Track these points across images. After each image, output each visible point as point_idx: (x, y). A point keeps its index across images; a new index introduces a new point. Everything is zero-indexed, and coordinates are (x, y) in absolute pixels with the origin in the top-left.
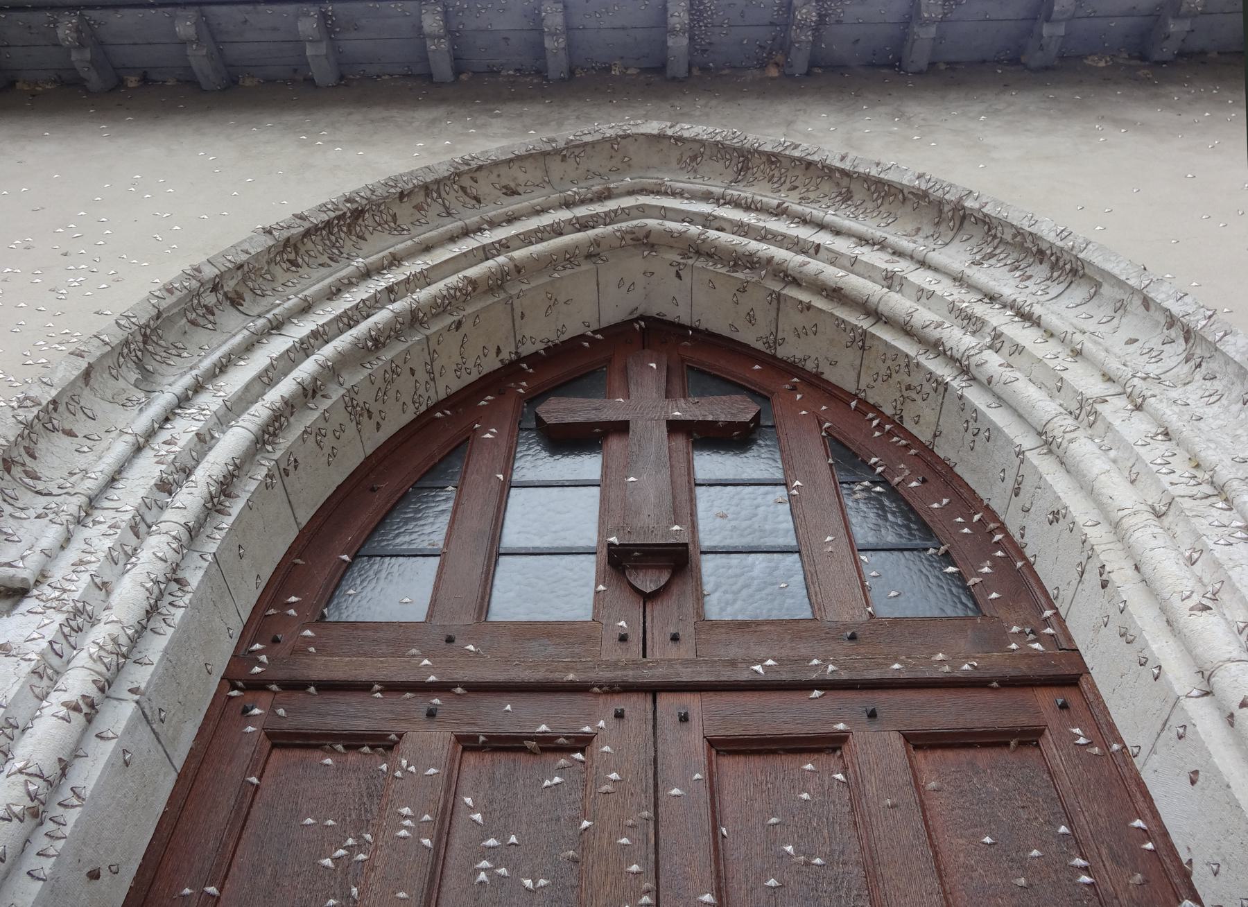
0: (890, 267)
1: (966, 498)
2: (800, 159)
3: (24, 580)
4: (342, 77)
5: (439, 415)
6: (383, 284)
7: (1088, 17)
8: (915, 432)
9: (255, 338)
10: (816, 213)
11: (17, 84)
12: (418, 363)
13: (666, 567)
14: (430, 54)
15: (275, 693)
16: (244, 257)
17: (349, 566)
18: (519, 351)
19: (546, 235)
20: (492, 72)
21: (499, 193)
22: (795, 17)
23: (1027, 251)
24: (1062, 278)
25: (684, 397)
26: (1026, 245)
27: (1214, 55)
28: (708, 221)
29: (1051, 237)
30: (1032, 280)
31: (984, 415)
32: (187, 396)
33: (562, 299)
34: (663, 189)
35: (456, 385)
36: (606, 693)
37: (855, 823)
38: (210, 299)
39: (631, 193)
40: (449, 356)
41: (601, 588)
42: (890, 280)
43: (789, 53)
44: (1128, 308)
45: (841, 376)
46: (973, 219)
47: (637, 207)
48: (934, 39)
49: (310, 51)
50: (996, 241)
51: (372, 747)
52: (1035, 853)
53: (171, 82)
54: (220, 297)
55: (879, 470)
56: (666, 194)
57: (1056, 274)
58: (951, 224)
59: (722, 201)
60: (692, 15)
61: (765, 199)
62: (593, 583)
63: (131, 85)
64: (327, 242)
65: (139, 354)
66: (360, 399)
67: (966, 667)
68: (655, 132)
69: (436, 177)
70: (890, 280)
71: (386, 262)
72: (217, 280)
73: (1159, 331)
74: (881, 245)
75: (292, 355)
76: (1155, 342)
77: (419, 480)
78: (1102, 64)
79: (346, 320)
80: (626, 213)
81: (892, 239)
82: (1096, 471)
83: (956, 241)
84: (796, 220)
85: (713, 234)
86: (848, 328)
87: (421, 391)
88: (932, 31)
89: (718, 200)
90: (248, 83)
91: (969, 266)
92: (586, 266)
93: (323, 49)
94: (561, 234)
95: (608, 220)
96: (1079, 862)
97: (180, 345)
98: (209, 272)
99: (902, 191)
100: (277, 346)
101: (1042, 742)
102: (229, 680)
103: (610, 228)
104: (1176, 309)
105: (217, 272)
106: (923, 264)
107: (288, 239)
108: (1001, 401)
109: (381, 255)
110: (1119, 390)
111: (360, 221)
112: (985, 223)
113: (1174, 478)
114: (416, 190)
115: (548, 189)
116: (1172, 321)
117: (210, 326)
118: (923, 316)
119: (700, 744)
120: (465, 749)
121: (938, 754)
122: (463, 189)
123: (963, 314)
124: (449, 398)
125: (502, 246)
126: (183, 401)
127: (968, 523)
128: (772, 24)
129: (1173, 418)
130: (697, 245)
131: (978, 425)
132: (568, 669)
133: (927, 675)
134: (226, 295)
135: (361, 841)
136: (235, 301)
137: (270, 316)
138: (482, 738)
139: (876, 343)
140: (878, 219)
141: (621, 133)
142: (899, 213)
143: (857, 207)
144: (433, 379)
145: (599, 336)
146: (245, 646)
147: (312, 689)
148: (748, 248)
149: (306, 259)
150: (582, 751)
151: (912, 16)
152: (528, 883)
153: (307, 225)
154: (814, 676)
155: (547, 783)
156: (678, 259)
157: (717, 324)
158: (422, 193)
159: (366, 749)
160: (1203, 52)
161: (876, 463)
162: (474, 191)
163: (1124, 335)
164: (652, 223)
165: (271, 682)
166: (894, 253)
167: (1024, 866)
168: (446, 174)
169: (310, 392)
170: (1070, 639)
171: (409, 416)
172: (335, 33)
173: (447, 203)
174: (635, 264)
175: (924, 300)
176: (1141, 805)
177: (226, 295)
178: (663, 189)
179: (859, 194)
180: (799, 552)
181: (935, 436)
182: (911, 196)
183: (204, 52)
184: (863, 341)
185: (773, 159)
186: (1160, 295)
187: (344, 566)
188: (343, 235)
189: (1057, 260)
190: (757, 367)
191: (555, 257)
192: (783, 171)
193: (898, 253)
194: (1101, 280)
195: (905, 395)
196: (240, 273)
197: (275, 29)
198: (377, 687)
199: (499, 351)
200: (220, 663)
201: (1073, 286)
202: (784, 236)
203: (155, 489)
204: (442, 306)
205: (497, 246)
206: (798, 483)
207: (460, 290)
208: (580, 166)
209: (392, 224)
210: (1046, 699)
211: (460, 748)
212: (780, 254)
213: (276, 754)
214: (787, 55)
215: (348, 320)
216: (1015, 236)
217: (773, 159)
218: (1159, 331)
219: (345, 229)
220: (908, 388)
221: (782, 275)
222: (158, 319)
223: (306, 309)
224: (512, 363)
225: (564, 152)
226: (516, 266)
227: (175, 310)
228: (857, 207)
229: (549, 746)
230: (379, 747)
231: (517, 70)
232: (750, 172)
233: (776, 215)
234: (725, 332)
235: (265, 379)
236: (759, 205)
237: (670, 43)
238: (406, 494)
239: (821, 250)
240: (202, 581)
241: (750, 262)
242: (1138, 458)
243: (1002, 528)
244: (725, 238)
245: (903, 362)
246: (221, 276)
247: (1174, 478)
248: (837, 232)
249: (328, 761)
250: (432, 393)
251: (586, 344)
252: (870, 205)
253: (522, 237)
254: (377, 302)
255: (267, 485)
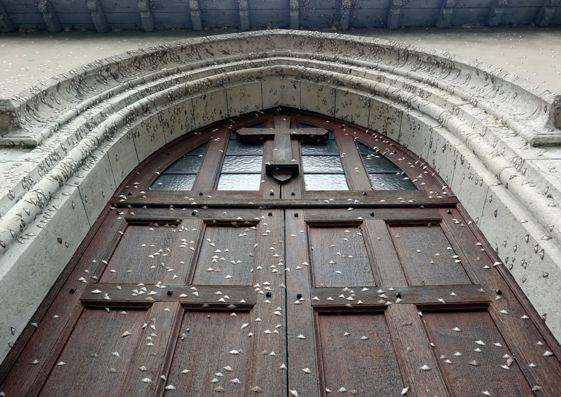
0: (379, 74)
1: (411, 156)
2: (343, 40)
3: (35, 141)
4: (155, 29)
5: (196, 133)
6: (174, 77)
7: (462, 8)
8: (392, 138)
9: (123, 89)
10: (350, 59)
11: (19, 30)
12: (188, 108)
13: (290, 174)
14: (192, 18)
15: (129, 208)
16: (119, 60)
17: (159, 176)
18: (229, 114)
19: (240, 68)
20: (218, 28)
21: (222, 53)
22: (342, 4)
23: (433, 64)
24: (446, 72)
25: (297, 128)
26: (432, 62)
27: (515, 25)
28: (306, 64)
29: (441, 56)
30: (435, 74)
31: (417, 119)
32: (96, 102)
33: (247, 94)
34: (288, 54)
35: (203, 124)
36: (265, 209)
37: (365, 246)
38: (105, 74)
39: (275, 56)
40: (200, 110)
41: (263, 181)
42: (379, 79)
43: (340, 20)
44: (471, 77)
45: (361, 121)
46: (411, 55)
47: (278, 60)
48: (399, 14)
49: (142, 15)
50: (421, 62)
51: (170, 225)
52: (437, 254)
53: (84, 30)
54: (109, 74)
55: (377, 151)
56: (289, 56)
57: (444, 70)
58: (403, 59)
59: (312, 58)
60: (300, 4)
61: (329, 56)
62: (260, 180)
63: (67, 30)
64: (152, 62)
65: (78, 86)
66: (165, 117)
67: (410, 201)
68: (285, 33)
69: (196, 43)
70: (379, 79)
71: (175, 71)
72: (109, 66)
73: (483, 82)
74: (376, 68)
75: (138, 96)
76: (482, 86)
77: (188, 153)
78: (469, 27)
79: (159, 88)
80: (273, 62)
81: (380, 65)
82: (458, 125)
83: (406, 65)
84: (342, 63)
85: (308, 69)
86: (364, 99)
87: (189, 122)
88: (398, 11)
89: (310, 57)
90: (116, 30)
91: (410, 71)
92: (256, 81)
93: (148, 15)
94: (246, 68)
95: (266, 65)
96: (455, 256)
97: (93, 88)
98: (105, 63)
99: (383, 48)
100: (132, 92)
101: (441, 224)
102: (111, 203)
103: (267, 67)
104: (489, 71)
105: (108, 63)
106: (392, 73)
107: (137, 57)
108: (423, 113)
109: (173, 68)
110: (468, 102)
111: (165, 56)
112: (416, 56)
113: (487, 122)
114: (188, 47)
115: (241, 53)
116: (487, 76)
117: (105, 84)
118: (392, 89)
119: (304, 224)
120: (207, 226)
121: (399, 228)
122: (207, 50)
123: (408, 86)
124: (200, 128)
125: (222, 70)
126: (94, 104)
127: (413, 164)
128: (333, 8)
129: (487, 106)
130: (302, 73)
131: (415, 125)
132: (249, 201)
133: (395, 203)
134: (111, 74)
135: (165, 251)
136: (115, 77)
137: (129, 82)
138: (214, 221)
139: (374, 102)
140: (375, 61)
141: (271, 33)
142: (383, 58)
143: (366, 57)
144: (194, 118)
145: (262, 112)
146: (117, 195)
147: (145, 207)
148: (323, 72)
149: (143, 67)
150: (255, 226)
151: (390, 6)
152: (233, 262)
153: (144, 53)
154: (349, 203)
155: (241, 235)
156: (295, 80)
157: (311, 107)
158: (190, 49)
159: (167, 225)
160: (510, 24)
161: (376, 149)
162: (211, 51)
163: (470, 86)
164: (284, 66)
165: (128, 204)
166: (381, 71)
167: (434, 258)
168: (200, 42)
169: (145, 109)
170: (452, 193)
171: (183, 132)
172: (153, 9)
173: (200, 55)
174: (277, 83)
175: (393, 84)
176: (479, 237)
177: (111, 74)
178: (288, 54)
179: (366, 50)
180: (344, 174)
181: (399, 136)
182: (387, 50)
183: (99, 15)
184: (369, 103)
185: (332, 41)
186: (482, 68)
187: (157, 176)
188: (158, 61)
189: (444, 65)
190: (328, 121)
191: (244, 76)
192: (336, 46)
193: (383, 70)
194: (460, 68)
195: (387, 122)
196: (117, 66)
197: (128, 7)
198: (171, 206)
199: (221, 112)
200: (109, 195)
201: (451, 73)
202: (337, 68)
203: (84, 125)
204: (198, 88)
205: (220, 70)
206: (344, 153)
207: (205, 83)
208: (254, 46)
209: (178, 60)
210: (443, 213)
211: (205, 225)
212: (335, 74)
213: (130, 228)
214: (339, 21)
215: (160, 88)
216: (428, 59)
217: (332, 41)
218: (483, 82)
219: (159, 58)
220: (388, 119)
221: (336, 82)
222: (85, 75)
223: (143, 82)
224: (226, 119)
225: (248, 39)
226: (228, 77)
227: (92, 74)
228: (366, 57)
229: (241, 224)
230: (172, 224)
231: (228, 27)
232: (323, 48)
233: (334, 61)
234: (314, 110)
235: (127, 102)
236: (327, 58)
237: (291, 14)
238: (182, 157)
239: (352, 71)
240: (102, 159)
241: (324, 78)
242: (475, 119)
243: (427, 164)
244: (314, 70)
245: (385, 108)
246: (110, 65)
247: (487, 122)
248: (359, 66)
249: (152, 229)
250: (193, 124)
251: (257, 115)
252: (371, 56)
253: (230, 67)
254: (172, 83)
255: (127, 137)
